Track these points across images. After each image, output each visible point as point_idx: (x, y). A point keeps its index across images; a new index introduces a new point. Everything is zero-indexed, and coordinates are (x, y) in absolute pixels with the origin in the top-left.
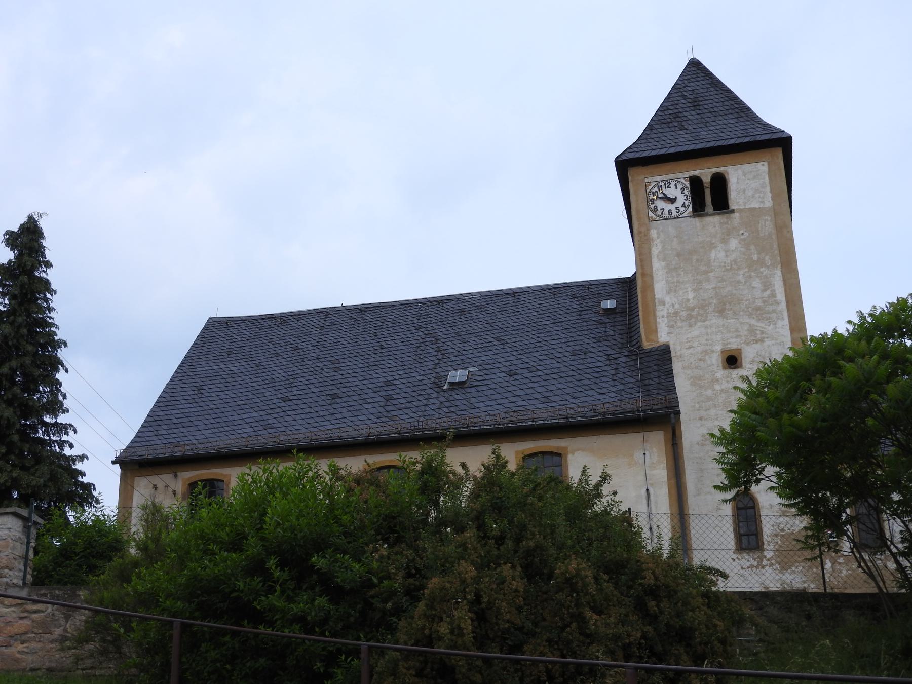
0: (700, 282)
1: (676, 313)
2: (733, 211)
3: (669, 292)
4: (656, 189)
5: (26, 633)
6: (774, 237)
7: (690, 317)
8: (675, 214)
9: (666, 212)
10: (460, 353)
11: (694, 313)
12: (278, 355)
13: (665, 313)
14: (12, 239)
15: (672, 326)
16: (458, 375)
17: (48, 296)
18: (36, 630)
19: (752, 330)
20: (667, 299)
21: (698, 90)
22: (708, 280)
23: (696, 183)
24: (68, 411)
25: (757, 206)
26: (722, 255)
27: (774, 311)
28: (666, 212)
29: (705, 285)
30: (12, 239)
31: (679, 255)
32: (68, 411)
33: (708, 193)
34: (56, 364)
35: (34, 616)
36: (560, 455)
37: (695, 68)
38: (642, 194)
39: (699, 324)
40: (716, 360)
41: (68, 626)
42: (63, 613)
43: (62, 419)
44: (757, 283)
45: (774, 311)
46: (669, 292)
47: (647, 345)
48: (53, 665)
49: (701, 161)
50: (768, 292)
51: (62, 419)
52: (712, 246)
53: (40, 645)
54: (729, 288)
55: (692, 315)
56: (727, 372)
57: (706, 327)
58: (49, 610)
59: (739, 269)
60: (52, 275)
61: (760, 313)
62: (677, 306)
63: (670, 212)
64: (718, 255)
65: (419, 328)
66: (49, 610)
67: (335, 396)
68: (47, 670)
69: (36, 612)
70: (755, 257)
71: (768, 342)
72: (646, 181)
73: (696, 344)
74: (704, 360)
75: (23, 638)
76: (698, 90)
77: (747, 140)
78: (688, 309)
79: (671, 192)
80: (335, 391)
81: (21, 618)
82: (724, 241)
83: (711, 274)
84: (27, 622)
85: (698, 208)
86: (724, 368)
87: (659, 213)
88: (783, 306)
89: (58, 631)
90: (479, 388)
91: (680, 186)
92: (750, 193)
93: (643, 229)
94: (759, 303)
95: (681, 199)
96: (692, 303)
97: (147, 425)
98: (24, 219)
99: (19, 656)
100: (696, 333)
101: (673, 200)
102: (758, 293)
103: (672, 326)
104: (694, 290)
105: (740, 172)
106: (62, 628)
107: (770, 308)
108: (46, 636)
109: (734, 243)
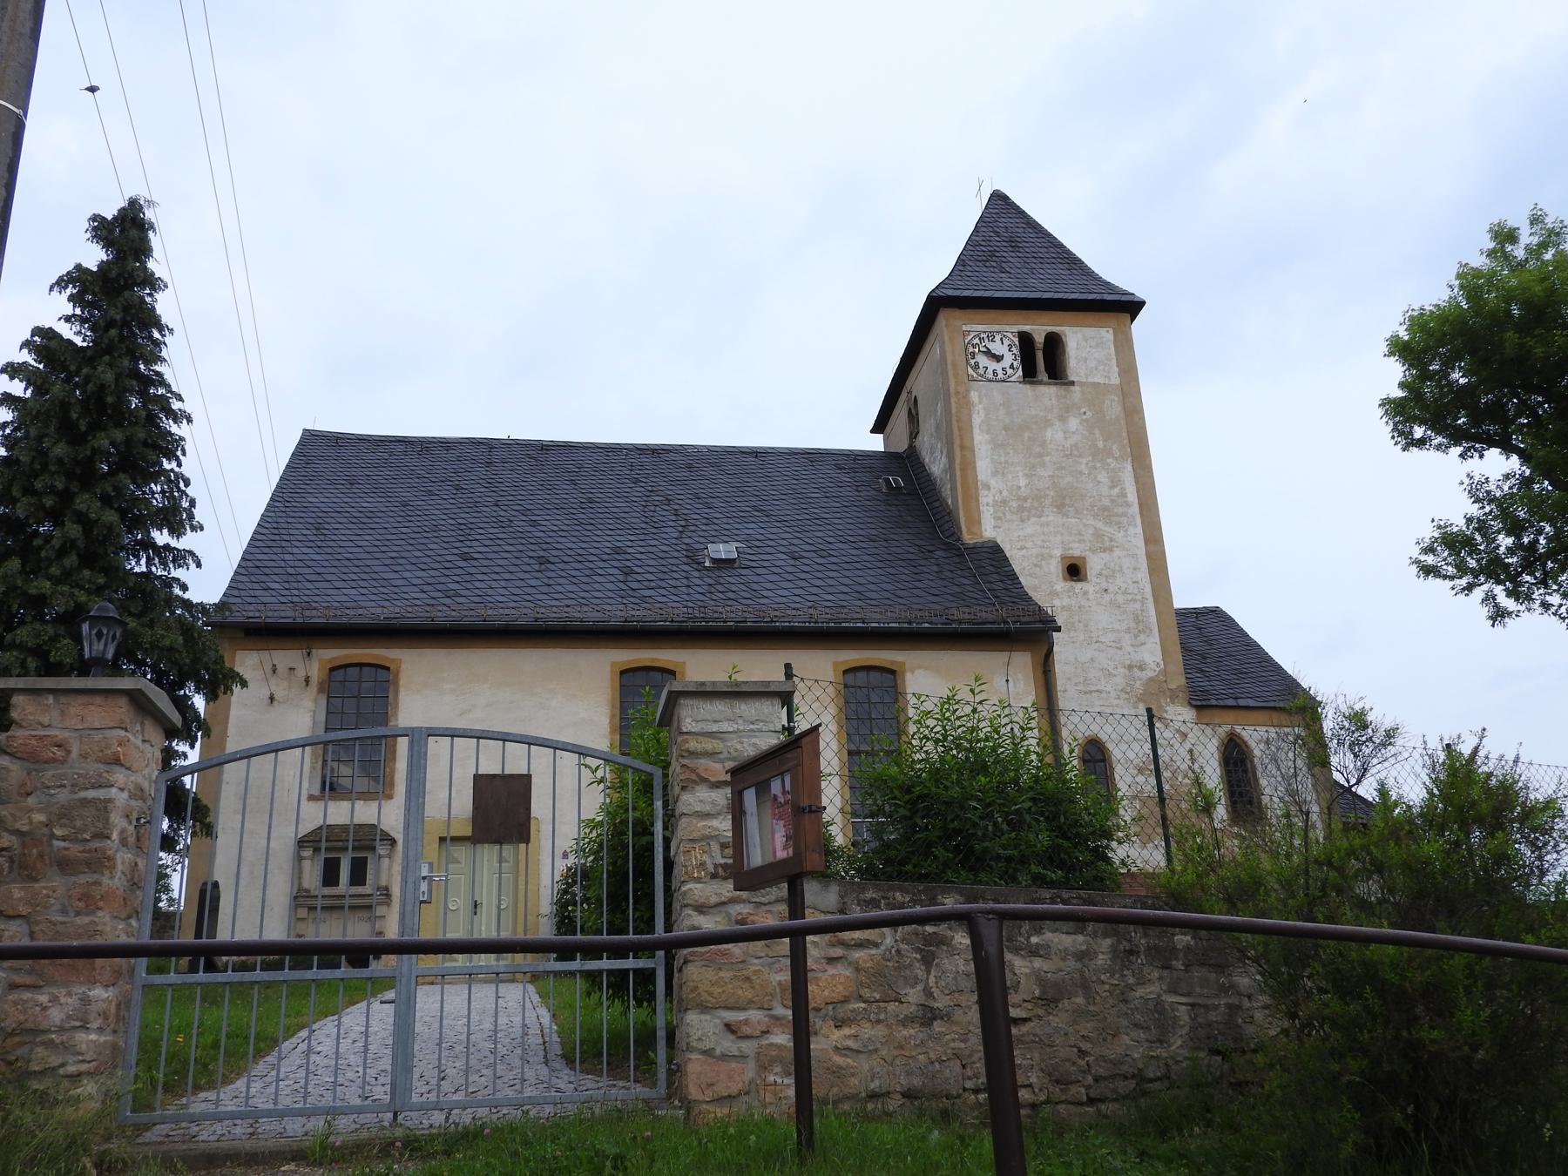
0: (1033, 467)
1: (1004, 502)
2: (1072, 383)
3: (995, 474)
4: (976, 341)
5: (846, 1000)
6: (1123, 422)
7: (1021, 509)
8: (1001, 376)
9: (990, 371)
10: (709, 521)
11: (1027, 505)
12: (431, 493)
13: (990, 500)
14: (102, 230)
15: (1000, 518)
16: (723, 550)
17: (156, 335)
18: (866, 993)
19: (1098, 535)
20: (993, 483)
21: (1004, 229)
22: (1043, 465)
23: (1025, 340)
24: (202, 528)
25: (1101, 381)
26: (1060, 435)
27: (1124, 515)
28: (1000, 372)
29: (1041, 472)
30: (102, 230)
31: (1006, 428)
32: (202, 528)
33: (1040, 356)
34: (171, 447)
35: (858, 955)
36: (893, 672)
37: (1000, 203)
38: (960, 348)
39: (1033, 519)
40: (1094, 565)
41: (932, 979)
42: (919, 950)
43: (187, 541)
44: (1103, 477)
45: (1124, 515)
46: (995, 474)
47: (968, 538)
48: (917, 1082)
49: (1033, 314)
50: (1117, 490)
51: (187, 541)
52: (1047, 423)
53: (880, 1031)
54: (1069, 479)
55: (1027, 506)
56: (1069, 584)
57: (1042, 525)
58: (889, 941)
59: (1081, 456)
60: (164, 305)
61: (1106, 514)
62: (1005, 493)
63: (994, 372)
64: (1054, 435)
65: (636, 481)
66: (889, 941)
67: (543, 561)
68: (904, 1095)
69: (861, 945)
70: (1100, 444)
71: (1117, 552)
73: (1029, 544)
74: (1040, 567)
75: (842, 1012)
76: (1004, 229)
77: (1091, 297)
78: (1019, 498)
79: (997, 347)
80: (541, 553)
81: (831, 960)
82: (1063, 419)
83: (1047, 459)
84: (842, 971)
85: (1029, 374)
86: (1065, 579)
87: (981, 371)
88: (1135, 509)
89: (914, 995)
90: (759, 571)
91: (1006, 342)
92: (1093, 364)
93: (961, 390)
94: (1106, 502)
95: (1008, 359)
96: (1024, 492)
97: (243, 571)
98: (123, 204)
99: (839, 1060)
100: (1029, 530)
101: (999, 358)
102: (1105, 490)
103: (1000, 518)
104: (1026, 475)
105: (1080, 335)
106: (920, 987)
107: (1120, 510)
108: (892, 1007)
109: (1074, 423)
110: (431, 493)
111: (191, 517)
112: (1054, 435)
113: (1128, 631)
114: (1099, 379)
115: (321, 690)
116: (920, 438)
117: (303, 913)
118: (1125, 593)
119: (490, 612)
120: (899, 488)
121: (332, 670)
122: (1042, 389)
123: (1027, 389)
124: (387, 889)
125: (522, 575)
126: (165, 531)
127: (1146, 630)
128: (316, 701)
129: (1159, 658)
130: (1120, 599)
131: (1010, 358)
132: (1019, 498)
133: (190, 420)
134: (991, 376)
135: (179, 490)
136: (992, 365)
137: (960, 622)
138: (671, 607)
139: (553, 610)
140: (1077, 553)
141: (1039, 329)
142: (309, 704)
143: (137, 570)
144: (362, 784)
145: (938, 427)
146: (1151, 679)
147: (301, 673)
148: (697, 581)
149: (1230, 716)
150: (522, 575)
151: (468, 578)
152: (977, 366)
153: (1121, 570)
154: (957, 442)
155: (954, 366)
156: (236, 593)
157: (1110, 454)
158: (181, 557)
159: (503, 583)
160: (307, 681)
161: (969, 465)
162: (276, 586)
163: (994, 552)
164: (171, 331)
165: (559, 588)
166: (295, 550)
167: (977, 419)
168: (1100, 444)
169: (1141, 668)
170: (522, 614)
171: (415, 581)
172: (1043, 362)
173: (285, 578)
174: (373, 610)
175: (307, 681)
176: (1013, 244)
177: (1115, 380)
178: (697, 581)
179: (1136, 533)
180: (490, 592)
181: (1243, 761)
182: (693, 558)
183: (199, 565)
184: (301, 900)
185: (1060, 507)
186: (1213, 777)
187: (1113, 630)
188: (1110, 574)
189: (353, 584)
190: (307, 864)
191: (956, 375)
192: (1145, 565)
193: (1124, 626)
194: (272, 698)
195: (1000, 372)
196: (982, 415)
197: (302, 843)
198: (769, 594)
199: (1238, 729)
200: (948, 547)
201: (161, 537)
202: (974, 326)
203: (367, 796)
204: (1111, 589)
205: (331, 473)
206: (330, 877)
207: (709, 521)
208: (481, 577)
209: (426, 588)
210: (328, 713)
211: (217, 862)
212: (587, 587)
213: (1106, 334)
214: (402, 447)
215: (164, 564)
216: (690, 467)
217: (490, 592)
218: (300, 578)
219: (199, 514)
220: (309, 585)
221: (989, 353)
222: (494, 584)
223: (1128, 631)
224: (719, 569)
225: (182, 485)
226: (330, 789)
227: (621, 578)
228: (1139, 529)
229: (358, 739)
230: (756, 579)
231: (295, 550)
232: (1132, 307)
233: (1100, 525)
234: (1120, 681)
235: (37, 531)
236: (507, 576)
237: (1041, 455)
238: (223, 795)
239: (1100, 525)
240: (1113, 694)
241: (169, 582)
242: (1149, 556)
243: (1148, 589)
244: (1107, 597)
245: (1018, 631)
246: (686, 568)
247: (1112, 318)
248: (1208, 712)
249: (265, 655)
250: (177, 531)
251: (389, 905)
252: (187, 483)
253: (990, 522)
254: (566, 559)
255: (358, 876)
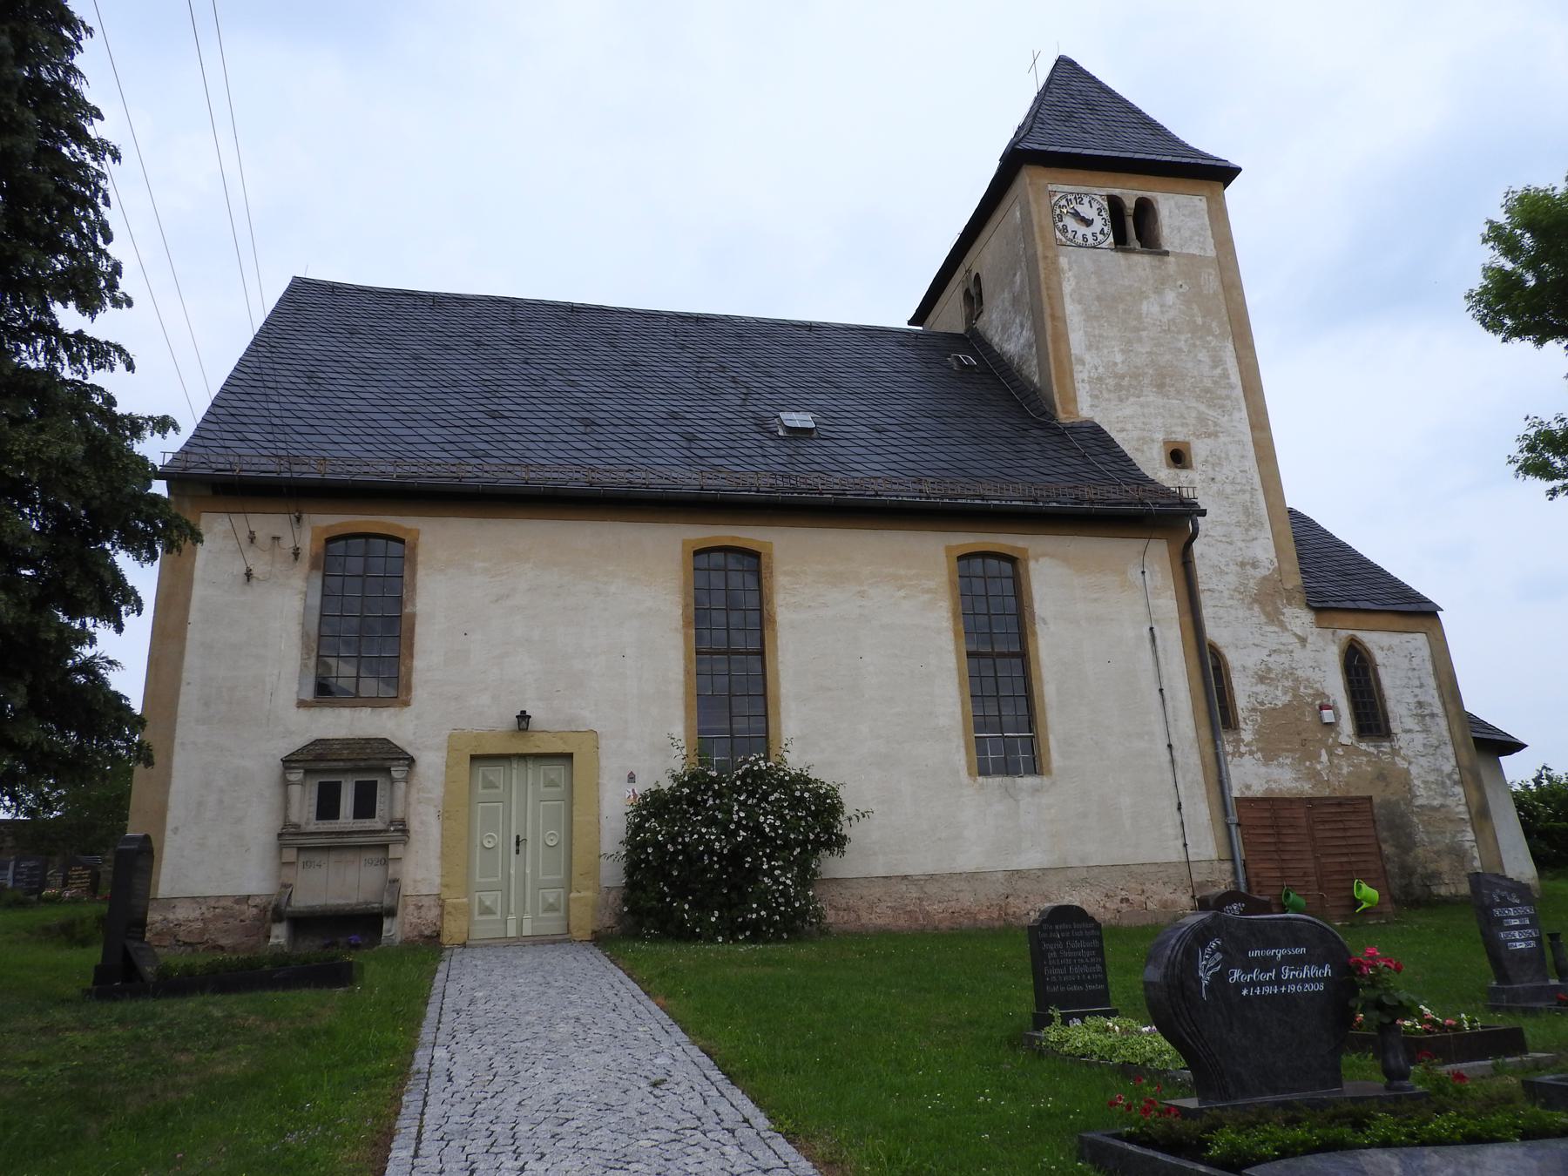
0: (1129, 342)
1: (1100, 379)
2: (1167, 253)
3: (1089, 347)
4: (1063, 202)
6: (1221, 297)
7: (1119, 387)
8: (1091, 241)
9: (1079, 235)
11: (1125, 383)
12: (447, 348)
13: (1085, 376)
15: (1096, 397)
16: (799, 419)
19: (1202, 419)
20: (1087, 358)
22: (1140, 340)
23: (1115, 205)
24: (130, 303)
25: (1196, 252)
26: (1156, 309)
28: (1090, 237)
29: (1137, 347)
31: (1099, 298)
32: (130, 303)
40: (1200, 450)
43: (105, 326)
44: (1203, 355)
45: (1228, 397)
46: (1089, 347)
47: (1063, 418)
49: (1123, 177)
50: (1219, 371)
51: (105, 326)
52: (1142, 296)
54: (1168, 357)
55: (1124, 385)
57: (1142, 406)
59: (1179, 332)
61: (1209, 396)
62: (1101, 370)
63: (1084, 236)
64: (1150, 307)
70: (1199, 321)
71: (1223, 439)
72: (1050, 188)
73: (1129, 427)
78: (1116, 376)
79: (1086, 211)
80: (586, 415)
82: (1158, 291)
83: (1144, 334)
85: (1121, 241)
86: (1169, 466)
87: (1070, 235)
88: (1239, 392)
92: (1187, 234)
93: (1050, 254)
94: (1208, 383)
95: (1099, 224)
96: (1121, 369)
100: (1128, 411)
101: (1088, 223)
103: (1096, 397)
104: (1122, 351)
105: (1172, 203)
107: (1224, 392)
109: (1170, 297)
110: (447, 348)
111: (113, 286)
112: (1150, 307)
113: (1238, 524)
114: (1194, 251)
115: (314, 566)
116: (984, 317)
117: (290, 855)
118: (1233, 483)
119: (532, 475)
120: (971, 366)
121: (329, 541)
122: (1136, 258)
123: (1119, 257)
124: (403, 822)
125: (564, 437)
126: (71, 304)
127: (1257, 524)
128: (307, 579)
129: (1272, 554)
130: (1229, 489)
131: (1100, 223)
132: (1116, 376)
133: (116, 157)
134: (1080, 240)
135: (96, 249)
136: (1082, 230)
137: (1092, 502)
138: (755, 473)
139: (614, 475)
140: (1180, 438)
141: (1130, 192)
142: (298, 582)
143: (33, 365)
144: (369, 686)
145: (1016, 300)
146: (1265, 578)
147: (288, 544)
148: (775, 452)
149: (1350, 619)
150: (564, 437)
151: (499, 437)
152: (1064, 230)
153: (1227, 458)
154: (1047, 312)
155: (1041, 228)
156: (199, 442)
157: (1210, 332)
158: (102, 353)
159: (543, 445)
160: (296, 553)
161: (1061, 337)
162: (257, 437)
163: (1095, 433)
164: (89, 31)
165: (612, 453)
166: (282, 399)
167: (1068, 287)
168: (1199, 321)
169: (1254, 565)
170: (573, 479)
171: (434, 439)
172: (1134, 229)
173: (269, 429)
174: (382, 468)
175: (296, 553)
176: (1091, 107)
177: (1211, 252)
178: (775, 452)
179: (1242, 416)
180: (528, 454)
181: (1366, 672)
182: (763, 426)
183: (130, 367)
184: (289, 837)
185: (1160, 387)
186: (1335, 686)
187: (1222, 524)
188: (1216, 461)
189: (356, 439)
190: (295, 790)
191: (1043, 238)
192: (1252, 452)
193: (1234, 519)
194: (249, 575)
195: (1090, 237)
196: (1073, 282)
197: (288, 762)
198: (860, 467)
199: (1360, 635)
200: (1043, 426)
201: (68, 317)
202: (1060, 187)
203: (376, 702)
204: (1218, 478)
205: (318, 324)
206: (327, 805)
207: (774, 390)
208: (515, 437)
209: (447, 447)
210: (323, 595)
211: (173, 789)
212: (645, 453)
213: (1200, 203)
214: (407, 301)
215: (75, 359)
216: (739, 336)
217: (528, 454)
218: (287, 430)
219: (125, 285)
220: (298, 438)
221: (1076, 215)
222: (532, 446)
223: (1238, 524)
224: (796, 439)
225: (100, 241)
226: (325, 692)
227: (684, 444)
228: (1244, 414)
229: (363, 638)
230: (840, 450)
231: (282, 399)
232: (1224, 174)
233: (1203, 408)
234: (1232, 579)
235: (87, 516)
236: (548, 438)
237: (1137, 330)
238: (182, 699)
239: (1203, 408)
240: (1226, 594)
241: (89, 390)
242: (1256, 443)
243: (1257, 479)
244: (1215, 487)
245: (1160, 515)
246: (758, 437)
247: (1206, 186)
248: (1326, 615)
249: (239, 520)
250: (89, 306)
251: (405, 843)
252: (108, 239)
253: (1086, 403)
254: (615, 421)
255: (365, 807)
